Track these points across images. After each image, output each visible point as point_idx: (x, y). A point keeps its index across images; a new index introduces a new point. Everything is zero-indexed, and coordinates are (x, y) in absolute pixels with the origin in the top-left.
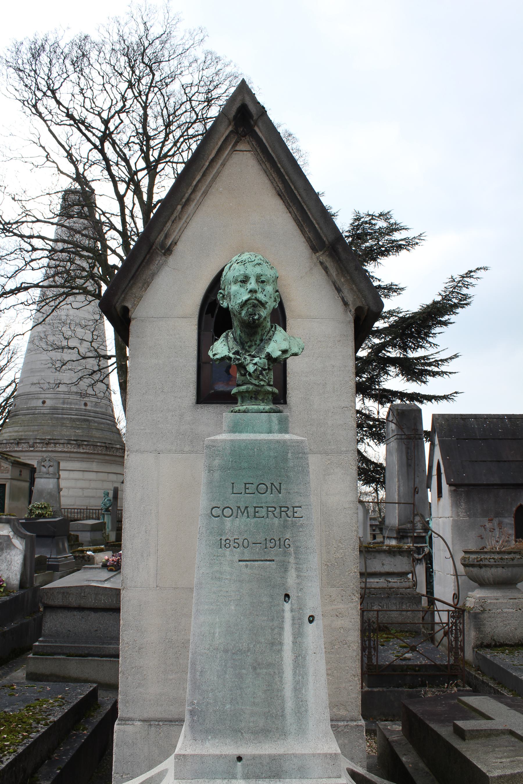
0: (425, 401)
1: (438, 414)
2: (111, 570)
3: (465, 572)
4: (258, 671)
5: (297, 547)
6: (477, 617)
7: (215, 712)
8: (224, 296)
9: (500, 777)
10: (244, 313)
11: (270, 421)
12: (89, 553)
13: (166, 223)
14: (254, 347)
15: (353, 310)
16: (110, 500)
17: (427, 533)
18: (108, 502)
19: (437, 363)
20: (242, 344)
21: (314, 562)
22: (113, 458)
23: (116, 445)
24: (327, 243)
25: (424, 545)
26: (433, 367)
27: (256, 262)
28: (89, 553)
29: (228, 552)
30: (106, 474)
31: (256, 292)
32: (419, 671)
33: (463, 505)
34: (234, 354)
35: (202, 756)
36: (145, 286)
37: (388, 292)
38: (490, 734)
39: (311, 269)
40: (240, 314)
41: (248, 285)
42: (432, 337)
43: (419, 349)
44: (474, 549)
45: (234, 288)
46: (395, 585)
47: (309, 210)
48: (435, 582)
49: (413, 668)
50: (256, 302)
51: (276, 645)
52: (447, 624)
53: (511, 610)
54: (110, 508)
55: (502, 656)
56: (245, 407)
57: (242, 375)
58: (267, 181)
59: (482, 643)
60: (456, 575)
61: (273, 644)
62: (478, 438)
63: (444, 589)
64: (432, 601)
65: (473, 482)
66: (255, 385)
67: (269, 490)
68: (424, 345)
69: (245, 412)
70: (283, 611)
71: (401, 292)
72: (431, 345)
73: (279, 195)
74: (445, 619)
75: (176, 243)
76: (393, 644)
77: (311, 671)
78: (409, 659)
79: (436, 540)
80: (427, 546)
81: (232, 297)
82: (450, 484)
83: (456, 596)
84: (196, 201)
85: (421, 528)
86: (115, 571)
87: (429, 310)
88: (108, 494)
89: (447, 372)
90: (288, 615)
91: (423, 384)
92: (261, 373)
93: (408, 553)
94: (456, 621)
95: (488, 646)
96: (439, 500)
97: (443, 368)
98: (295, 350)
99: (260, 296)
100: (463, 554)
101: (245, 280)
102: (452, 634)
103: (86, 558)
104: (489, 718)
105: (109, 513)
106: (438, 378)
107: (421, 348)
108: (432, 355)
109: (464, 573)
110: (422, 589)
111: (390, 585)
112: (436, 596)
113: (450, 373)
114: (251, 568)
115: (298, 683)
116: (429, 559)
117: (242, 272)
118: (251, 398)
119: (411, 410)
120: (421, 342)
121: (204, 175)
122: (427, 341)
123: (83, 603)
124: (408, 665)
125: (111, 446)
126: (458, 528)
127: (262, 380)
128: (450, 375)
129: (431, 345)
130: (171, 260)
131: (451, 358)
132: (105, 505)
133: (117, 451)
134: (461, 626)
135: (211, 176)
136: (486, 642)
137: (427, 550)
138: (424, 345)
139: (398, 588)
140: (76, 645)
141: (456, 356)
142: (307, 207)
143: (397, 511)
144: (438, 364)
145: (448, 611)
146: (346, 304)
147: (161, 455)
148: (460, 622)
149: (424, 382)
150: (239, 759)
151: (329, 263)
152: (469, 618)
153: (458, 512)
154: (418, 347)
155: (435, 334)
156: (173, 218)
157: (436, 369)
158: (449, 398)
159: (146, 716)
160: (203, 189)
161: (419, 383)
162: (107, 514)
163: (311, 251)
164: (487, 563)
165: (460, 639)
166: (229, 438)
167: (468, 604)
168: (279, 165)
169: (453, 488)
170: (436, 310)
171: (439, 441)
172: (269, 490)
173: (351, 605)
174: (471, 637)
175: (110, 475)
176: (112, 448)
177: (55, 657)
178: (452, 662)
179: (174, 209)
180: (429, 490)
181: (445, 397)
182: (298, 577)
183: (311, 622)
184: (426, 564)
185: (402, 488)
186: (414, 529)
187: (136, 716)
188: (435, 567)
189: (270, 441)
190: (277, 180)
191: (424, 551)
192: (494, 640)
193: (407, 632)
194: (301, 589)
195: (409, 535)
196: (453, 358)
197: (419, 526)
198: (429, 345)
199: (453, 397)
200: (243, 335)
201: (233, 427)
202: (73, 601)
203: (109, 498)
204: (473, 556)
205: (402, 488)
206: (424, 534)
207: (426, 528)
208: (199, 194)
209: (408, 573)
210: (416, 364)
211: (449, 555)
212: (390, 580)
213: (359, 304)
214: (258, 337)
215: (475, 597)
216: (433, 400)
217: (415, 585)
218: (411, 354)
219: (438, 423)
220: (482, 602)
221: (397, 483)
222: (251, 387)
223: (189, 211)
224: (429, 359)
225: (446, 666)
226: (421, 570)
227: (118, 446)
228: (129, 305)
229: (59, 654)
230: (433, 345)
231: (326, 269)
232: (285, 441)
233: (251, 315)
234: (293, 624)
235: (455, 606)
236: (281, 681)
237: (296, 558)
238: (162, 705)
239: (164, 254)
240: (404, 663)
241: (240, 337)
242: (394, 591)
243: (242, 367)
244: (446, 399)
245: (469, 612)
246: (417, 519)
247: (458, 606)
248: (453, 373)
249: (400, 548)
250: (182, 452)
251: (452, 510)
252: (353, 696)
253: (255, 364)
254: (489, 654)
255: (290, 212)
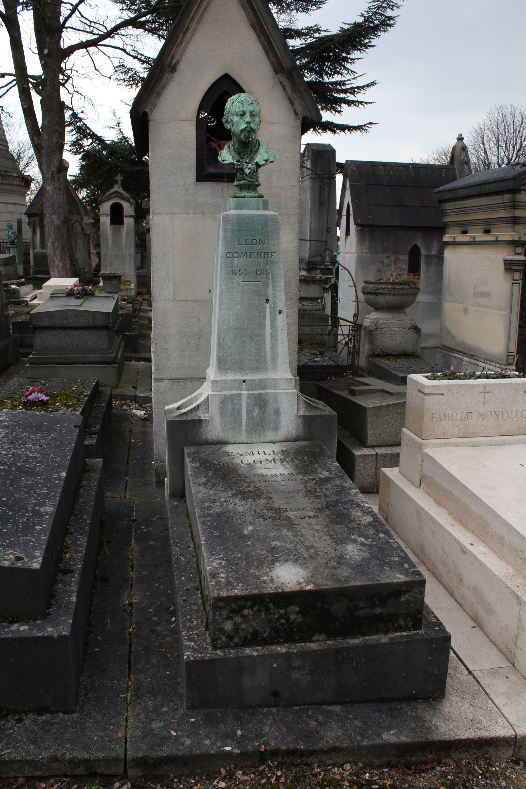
0: (338, 131)
1: (351, 161)
2: (78, 298)
3: (365, 299)
4: (253, 339)
5: (273, 274)
6: (371, 334)
7: (231, 359)
8: (227, 121)
9: (373, 408)
10: (242, 136)
11: (258, 203)
12: (13, 286)
13: (172, 48)
14: (246, 156)
15: (301, 119)
16: (14, 233)
17: (334, 265)
18: (12, 235)
19: (352, 91)
20: (239, 153)
21: (281, 282)
22: (10, 188)
23: (12, 172)
24: (286, 68)
25: (331, 276)
26: (348, 94)
27: (250, 102)
28: (13, 286)
29: (236, 277)
30: (4, 205)
31: (250, 123)
32: (325, 369)
33: (367, 243)
34: (236, 161)
35: (225, 380)
36: (159, 96)
37: (307, 5)
38: (370, 392)
39: (274, 86)
40: (240, 136)
41: (245, 117)
42: (351, 63)
43: (336, 75)
44: (373, 280)
45: (236, 119)
46: (308, 308)
47: (274, 42)
48: (339, 308)
49: (321, 367)
50: (250, 129)
51: (262, 325)
52: (348, 336)
53: (398, 329)
54: (16, 241)
55: (387, 362)
56: (243, 194)
57: (240, 174)
58: (244, 14)
59: (373, 354)
60: (357, 302)
61: (260, 325)
62: (385, 184)
63: (346, 310)
64: (336, 320)
65: (376, 223)
66: (249, 181)
67: (258, 243)
68: (341, 71)
69: (243, 197)
70: (266, 308)
71: (321, 6)
72: (348, 72)
73: (252, 26)
74: (346, 332)
75: (178, 63)
76: (306, 353)
77: (280, 338)
78: (318, 362)
79: (341, 271)
80: (333, 278)
81: (234, 124)
82: (357, 224)
83: (356, 315)
84: (192, 29)
85: (329, 261)
86: (81, 298)
87: (349, 33)
88: (11, 227)
89: (363, 102)
90: (268, 310)
91: (337, 113)
92: (253, 174)
93: (320, 282)
94: (355, 333)
95: (378, 356)
96: (346, 238)
97: (359, 97)
98: (272, 159)
99: (252, 125)
100: (364, 284)
101: (243, 114)
102: (351, 343)
103: (11, 291)
104: (371, 386)
105: (15, 246)
106: (353, 108)
107: (338, 74)
108: (349, 80)
109: (364, 300)
110: (328, 311)
111: (304, 307)
112: (339, 315)
113: (366, 103)
114: (249, 285)
115: (273, 344)
116: (335, 288)
117: (241, 109)
118: (246, 188)
119: (325, 151)
120: (338, 68)
121: (198, 8)
122: (344, 67)
123: (65, 323)
124: (317, 366)
125: (7, 174)
126: (361, 263)
127: (253, 178)
128: (365, 105)
129: (348, 72)
130: (176, 76)
131: (368, 86)
132: (9, 238)
133: (14, 180)
134: (358, 337)
135: (203, 8)
136: (376, 352)
137: (333, 281)
138: (341, 71)
139: (310, 310)
140: (63, 356)
141: (374, 83)
142: (273, 39)
143: (308, 245)
144: (355, 92)
145: (349, 326)
146: (296, 113)
147: (175, 216)
148: (357, 335)
149: (339, 112)
150: (244, 381)
151: (286, 83)
152: (365, 334)
153: (362, 249)
154: (335, 73)
155: (354, 59)
156: (177, 44)
157: (351, 97)
158: (363, 129)
159: (170, 377)
160: (197, 19)
161: (334, 112)
162: (12, 247)
163: (273, 72)
164: (382, 291)
165: (356, 347)
166: (236, 213)
167: (365, 324)
168: (253, 3)
169: (359, 228)
170: (356, 33)
171: (350, 185)
172: (258, 243)
173: (293, 310)
174: (365, 348)
175: (8, 205)
176: (8, 176)
177: (48, 365)
178: (350, 363)
179: (178, 36)
180: (338, 228)
181: (359, 128)
182: (273, 290)
183: (280, 313)
184: (332, 293)
185: (313, 224)
186: (323, 262)
187: (165, 377)
188: (340, 295)
189: (258, 215)
190: (251, 13)
191: (330, 281)
192: (383, 351)
193: (316, 344)
194: (275, 297)
195: (318, 267)
196: (370, 86)
197: (328, 259)
198: (346, 72)
199: (367, 128)
200: (240, 148)
201: (237, 206)
202: (58, 322)
203: (13, 231)
204: (371, 286)
205: (313, 224)
206: (331, 267)
207: (334, 261)
208: (194, 23)
209: (318, 298)
210: (331, 91)
211: (352, 284)
212: (304, 303)
213: (305, 114)
214: (249, 150)
215: (370, 318)
216: (346, 130)
217: (324, 308)
218: (326, 79)
219: (351, 169)
220: (376, 322)
221: (309, 220)
222: (247, 182)
223: (187, 37)
224: (346, 85)
225: (345, 366)
226: (328, 297)
227: (15, 174)
228: (148, 111)
229: (50, 363)
230: (350, 72)
231: (284, 87)
232: (267, 215)
233: (247, 138)
234: (271, 315)
235: (354, 323)
236: (264, 344)
237: (272, 280)
238: (180, 370)
239: (171, 71)
240: (314, 364)
241: (238, 149)
242: (307, 313)
243: (242, 170)
244: (360, 129)
245: (365, 330)
246: (327, 252)
247: (357, 323)
248: (368, 103)
249: (313, 278)
250: (188, 214)
251: (357, 247)
252: (293, 363)
253: (249, 168)
254: (377, 361)
255: (260, 41)
